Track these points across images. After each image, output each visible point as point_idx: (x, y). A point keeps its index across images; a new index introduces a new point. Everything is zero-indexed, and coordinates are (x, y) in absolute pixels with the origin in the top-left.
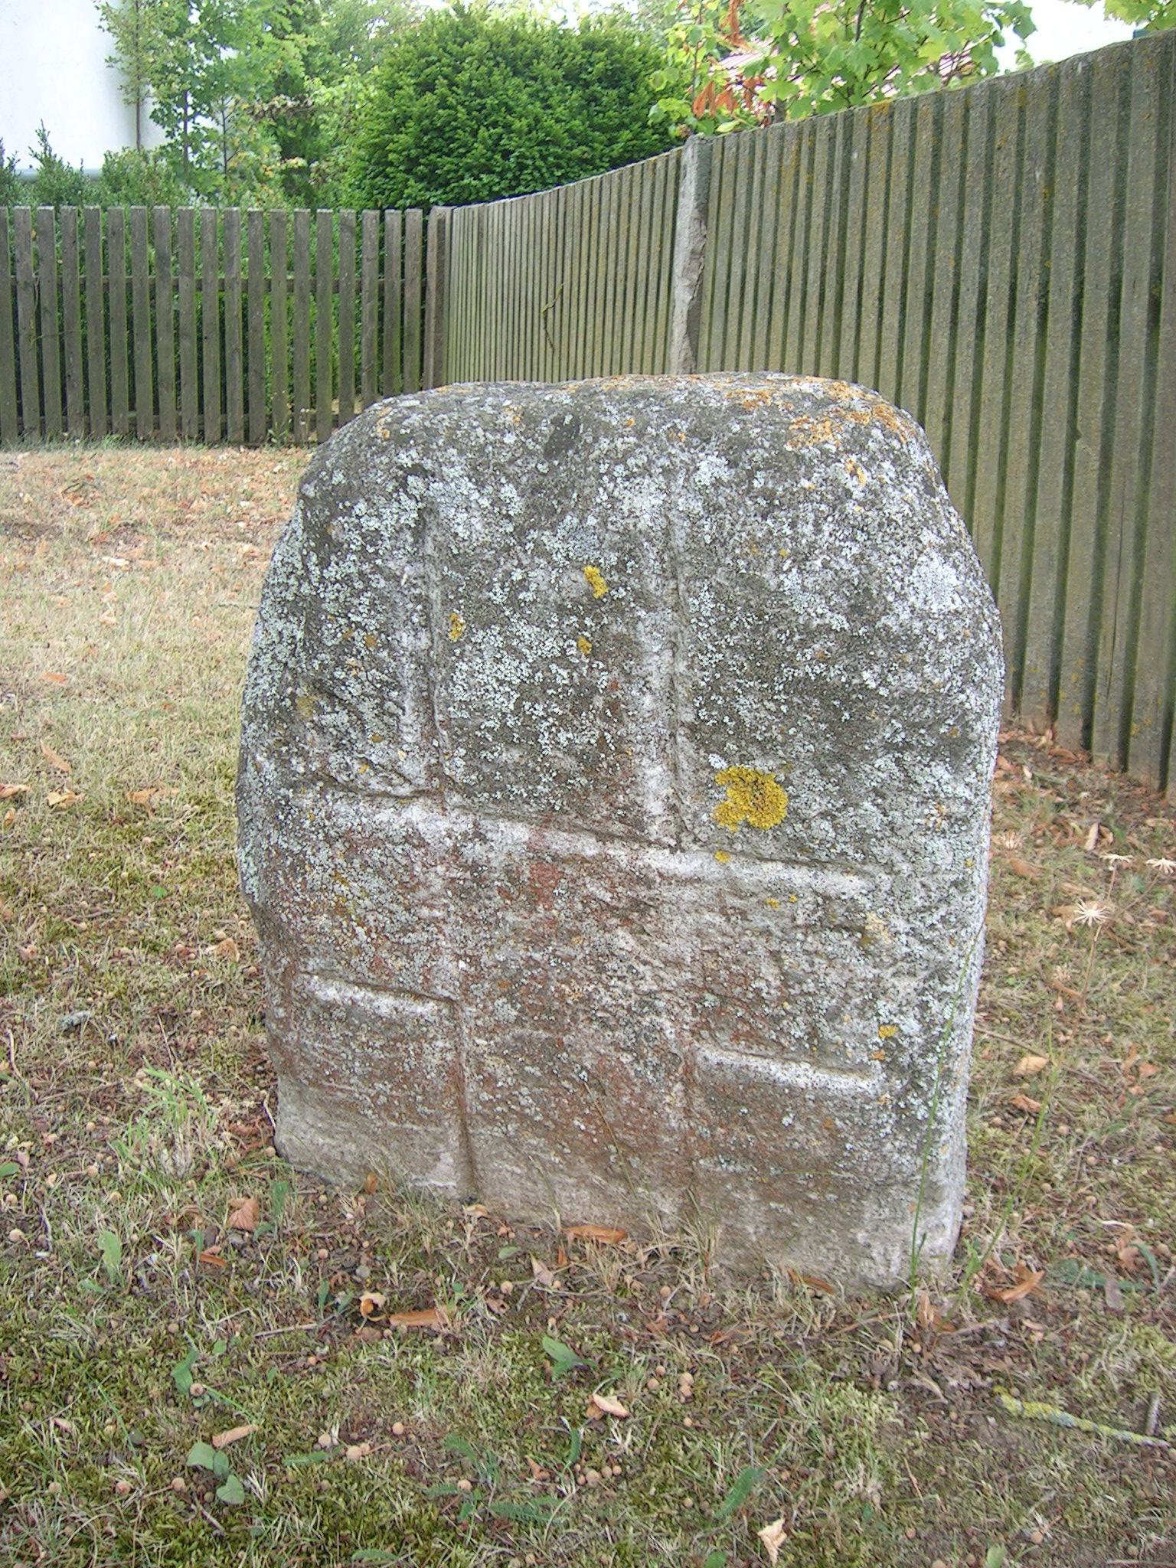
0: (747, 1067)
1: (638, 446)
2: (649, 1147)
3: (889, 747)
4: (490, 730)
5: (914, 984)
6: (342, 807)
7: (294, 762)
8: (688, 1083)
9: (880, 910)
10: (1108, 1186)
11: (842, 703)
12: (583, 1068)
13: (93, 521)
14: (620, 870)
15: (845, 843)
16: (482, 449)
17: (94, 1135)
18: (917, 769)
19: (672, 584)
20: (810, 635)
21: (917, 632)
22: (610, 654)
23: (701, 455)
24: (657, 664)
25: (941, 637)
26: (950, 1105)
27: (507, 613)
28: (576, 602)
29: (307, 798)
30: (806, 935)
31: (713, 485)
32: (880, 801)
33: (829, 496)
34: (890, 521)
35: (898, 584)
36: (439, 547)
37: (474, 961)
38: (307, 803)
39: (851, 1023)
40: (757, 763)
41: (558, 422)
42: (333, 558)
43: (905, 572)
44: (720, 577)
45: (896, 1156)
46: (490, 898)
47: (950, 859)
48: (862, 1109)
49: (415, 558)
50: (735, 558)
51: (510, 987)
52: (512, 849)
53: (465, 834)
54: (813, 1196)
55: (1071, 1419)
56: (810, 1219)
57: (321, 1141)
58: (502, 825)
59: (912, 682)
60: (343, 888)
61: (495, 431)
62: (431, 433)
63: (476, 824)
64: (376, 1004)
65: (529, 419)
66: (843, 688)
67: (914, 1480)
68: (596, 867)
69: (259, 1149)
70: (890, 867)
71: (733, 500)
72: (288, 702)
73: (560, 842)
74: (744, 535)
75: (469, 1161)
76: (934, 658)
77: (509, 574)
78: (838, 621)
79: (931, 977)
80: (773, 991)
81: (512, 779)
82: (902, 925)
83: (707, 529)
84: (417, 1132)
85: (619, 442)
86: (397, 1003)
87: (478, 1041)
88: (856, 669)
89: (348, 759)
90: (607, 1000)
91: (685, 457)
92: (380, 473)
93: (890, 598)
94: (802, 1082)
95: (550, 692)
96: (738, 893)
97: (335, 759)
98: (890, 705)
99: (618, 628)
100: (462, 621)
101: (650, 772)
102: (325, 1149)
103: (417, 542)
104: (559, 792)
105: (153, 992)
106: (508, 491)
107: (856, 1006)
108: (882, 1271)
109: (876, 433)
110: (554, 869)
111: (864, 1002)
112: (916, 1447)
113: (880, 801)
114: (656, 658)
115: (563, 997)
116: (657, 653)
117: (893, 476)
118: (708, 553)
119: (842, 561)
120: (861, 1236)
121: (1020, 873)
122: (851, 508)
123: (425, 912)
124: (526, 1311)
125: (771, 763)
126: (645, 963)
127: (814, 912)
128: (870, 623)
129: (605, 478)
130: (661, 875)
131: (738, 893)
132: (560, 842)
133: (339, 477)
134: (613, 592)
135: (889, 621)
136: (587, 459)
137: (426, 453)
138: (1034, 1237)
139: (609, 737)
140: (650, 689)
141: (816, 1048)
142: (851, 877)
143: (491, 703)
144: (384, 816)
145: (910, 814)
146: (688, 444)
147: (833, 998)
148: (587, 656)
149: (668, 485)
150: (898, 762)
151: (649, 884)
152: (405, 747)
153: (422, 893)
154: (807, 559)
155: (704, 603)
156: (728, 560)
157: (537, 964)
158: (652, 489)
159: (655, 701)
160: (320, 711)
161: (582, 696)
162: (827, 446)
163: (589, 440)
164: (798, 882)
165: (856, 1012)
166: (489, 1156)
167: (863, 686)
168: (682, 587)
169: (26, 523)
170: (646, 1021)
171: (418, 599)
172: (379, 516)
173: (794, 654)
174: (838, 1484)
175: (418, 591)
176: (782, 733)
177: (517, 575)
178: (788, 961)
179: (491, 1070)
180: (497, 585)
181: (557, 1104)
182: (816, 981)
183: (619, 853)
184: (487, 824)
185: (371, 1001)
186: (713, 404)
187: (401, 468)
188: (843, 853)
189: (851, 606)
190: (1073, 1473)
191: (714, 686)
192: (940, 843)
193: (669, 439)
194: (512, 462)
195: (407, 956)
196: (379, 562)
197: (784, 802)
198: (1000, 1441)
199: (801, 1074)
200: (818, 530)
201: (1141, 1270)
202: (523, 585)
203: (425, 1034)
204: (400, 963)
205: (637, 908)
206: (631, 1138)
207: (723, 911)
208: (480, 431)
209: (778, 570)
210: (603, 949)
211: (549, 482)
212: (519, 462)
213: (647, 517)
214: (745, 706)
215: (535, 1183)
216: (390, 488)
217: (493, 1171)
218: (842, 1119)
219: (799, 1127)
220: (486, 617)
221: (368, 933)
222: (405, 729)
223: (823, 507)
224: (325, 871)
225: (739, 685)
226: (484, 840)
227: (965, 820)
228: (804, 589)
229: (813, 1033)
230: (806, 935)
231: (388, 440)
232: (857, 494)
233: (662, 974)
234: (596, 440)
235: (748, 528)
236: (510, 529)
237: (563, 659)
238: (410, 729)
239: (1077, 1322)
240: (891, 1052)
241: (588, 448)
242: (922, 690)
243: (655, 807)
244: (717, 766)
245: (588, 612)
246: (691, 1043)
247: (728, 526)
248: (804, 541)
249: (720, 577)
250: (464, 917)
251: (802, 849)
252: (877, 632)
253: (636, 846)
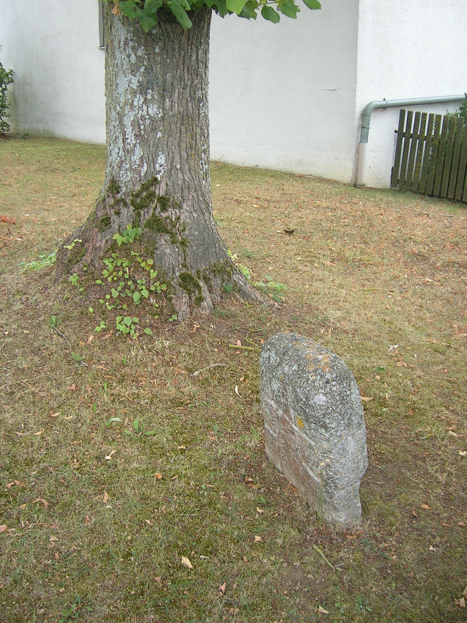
106: (278, 358)
109: (320, 370)
122: (309, 382)
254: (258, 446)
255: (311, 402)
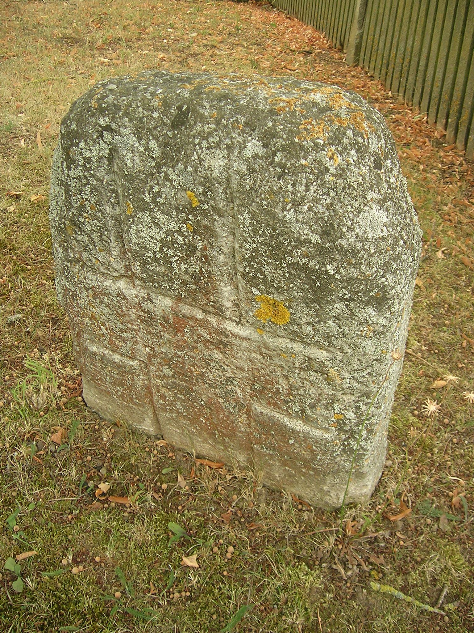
0: (274, 417)
1: (216, 130)
2: (232, 435)
3: (342, 299)
4: (150, 257)
5: (353, 398)
6: (90, 275)
7: (69, 251)
8: (249, 416)
9: (336, 368)
10: (459, 456)
11: (316, 278)
12: (202, 400)
13: (100, 37)
14: (213, 327)
15: (319, 337)
16: (141, 120)
17: (8, 383)
18: (357, 310)
19: (232, 205)
20: (300, 243)
21: (358, 248)
22: (202, 233)
23: (250, 138)
24: (225, 240)
25: (372, 251)
26: (371, 443)
27: (152, 207)
28: (184, 207)
29: (76, 268)
30: (300, 371)
31: (253, 157)
32: (337, 321)
33: (316, 171)
34: (350, 186)
35: (350, 223)
36: (119, 168)
37: (153, 349)
38: (76, 270)
39: (320, 410)
40: (275, 296)
41: (180, 108)
42: (72, 166)
43: (355, 216)
44: (253, 208)
45: (342, 462)
46: (156, 326)
47: (374, 349)
48: (325, 445)
49: (109, 172)
50: (261, 200)
51: (168, 362)
52: (164, 309)
53: (143, 298)
54: (304, 470)
55: (402, 595)
56: (303, 478)
57: (98, 401)
58: (159, 297)
59: (353, 272)
60: (93, 309)
61: (148, 110)
62: (117, 107)
63: (148, 294)
64: (113, 357)
65: (166, 105)
66: (317, 271)
67: (320, 619)
68: (203, 324)
69: (75, 397)
70: (342, 350)
71: (263, 167)
72: (63, 226)
73: (186, 309)
74: (267, 187)
75: (157, 421)
76: (367, 262)
77: (152, 188)
78: (315, 238)
79: (362, 396)
80: (285, 391)
81: (162, 279)
82: (347, 375)
83: (248, 181)
84: (135, 408)
85: (206, 127)
86: (122, 358)
87: (157, 380)
88: (324, 264)
89: (90, 256)
90: (211, 377)
91: (240, 139)
92: (91, 127)
93: (344, 230)
94: (298, 428)
95: (175, 246)
96: (267, 348)
97: (85, 255)
98: (342, 283)
99: (205, 222)
100: (132, 207)
101: (224, 289)
102: (100, 405)
103: (110, 164)
104: (183, 289)
105: (51, 305)
106: (153, 144)
107: (324, 404)
108: (335, 501)
109: (350, 133)
110: (184, 320)
111: (327, 403)
112: (325, 602)
113: (337, 321)
114: (225, 239)
115: (191, 372)
116: (225, 237)
117: (355, 159)
118: (249, 195)
119: (320, 207)
120: (325, 488)
121: (466, 264)
122: (328, 178)
123: (130, 325)
124: (170, 501)
125: (281, 297)
126: (228, 366)
127: (304, 363)
128: (333, 241)
129: (197, 146)
130: (232, 334)
131: (267, 348)
132: (186, 309)
133: (74, 126)
134: (202, 205)
135: (343, 242)
136: (189, 134)
137: (113, 119)
138: (416, 484)
139: (204, 270)
140: (223, 252)
141: (303, 416)
142: (323, 351)
143: (148, 246)
144: (108, 283)
145: (351, 329)
146: (243, 131)
147: (312, 399)
148: (192, 232)
149: (229, 155)
150: (347, 306)
151: (227, 336)
152: (113, 256)
153: (127, 318)
154: (300, 204)
155: (246, 218)
156: (258, 200)
157: (179, 357)
158: (220, 156)
159: (226, 258)
160: (77, 234)
161: (191, 250)
162: (318, 141)
163: (192, 123)
164: (296, 349)
165: (323, 407)
166: (165, 423)
167: (327, 273)
168: (235, 208)
169: (72, 37)
170: (229, 388)
171: (113, 191)
172: (90, 150)
173: (292, 251)
174: (284, 618)
175: (112, 188)
176: (286, 285)
177: (156, 189)
178: (291, 380)
179: (163, 393)
180: (146, 192)
181: (193, 410)
182: (305, 391)
183: (213, 320)
184: (153, 295)
185: (111, 355)
186: (261, 107)
187: (100, 126)
188: (318, 341)
189: (323, 231)
190: (395, 625)
191: (253, 258)
192: (369, 342)
193: (233, 128)
194: (155, 128)
195: (124, 341)
196: (92, 172)
197: (288, 315)
198: (366, 602)
199: (298, 425)
200: (307, 189)
201: (460, 510)
202: (159, 194)
203: (135, 373)
204: (121, 344)
205: (223, 343)
206: (224, 430)
207: (261, 354)
208: (141, 109)
209: (284, 209)
210: (207, 357)
211: (172, 142)
212: (159, 129)
213: (217, 171)
214: (267, 270)
215: (186, 437)
216: (95, 137)
217: (168, 429)
218: (316, 447)
219: (296, 445)
220: (143, 207)
221: (106, 329)
222: (112, 249)
223: (311, 177)
224: (85, 301)
225: (265, 260)
226: (152, 302)
227: (383, 333)
228: (297, 221)
229: (303, 411)
230: (300, 371)
231: (96, 109)
232: (332, 170)
233: (235, 371)
234: (195, 123)
235: (269, 184)
236: (153, 164)
237: (179, 232)
238: (114, 249)
239: (421, 538)
240: (340, 425)
241: (191, 127)
242: (359, 277)
243: (228, 304)
244: (256, 293)
245: (190, 213)
246: (250, 400)
247: (259, 182)
248: (299, 195)
249: (253, 208)
250: (146, 331)
251: (297, 336)
252: (336, 247)
253: (220, 318)
254: (59, 393)
255: (348, 240)
